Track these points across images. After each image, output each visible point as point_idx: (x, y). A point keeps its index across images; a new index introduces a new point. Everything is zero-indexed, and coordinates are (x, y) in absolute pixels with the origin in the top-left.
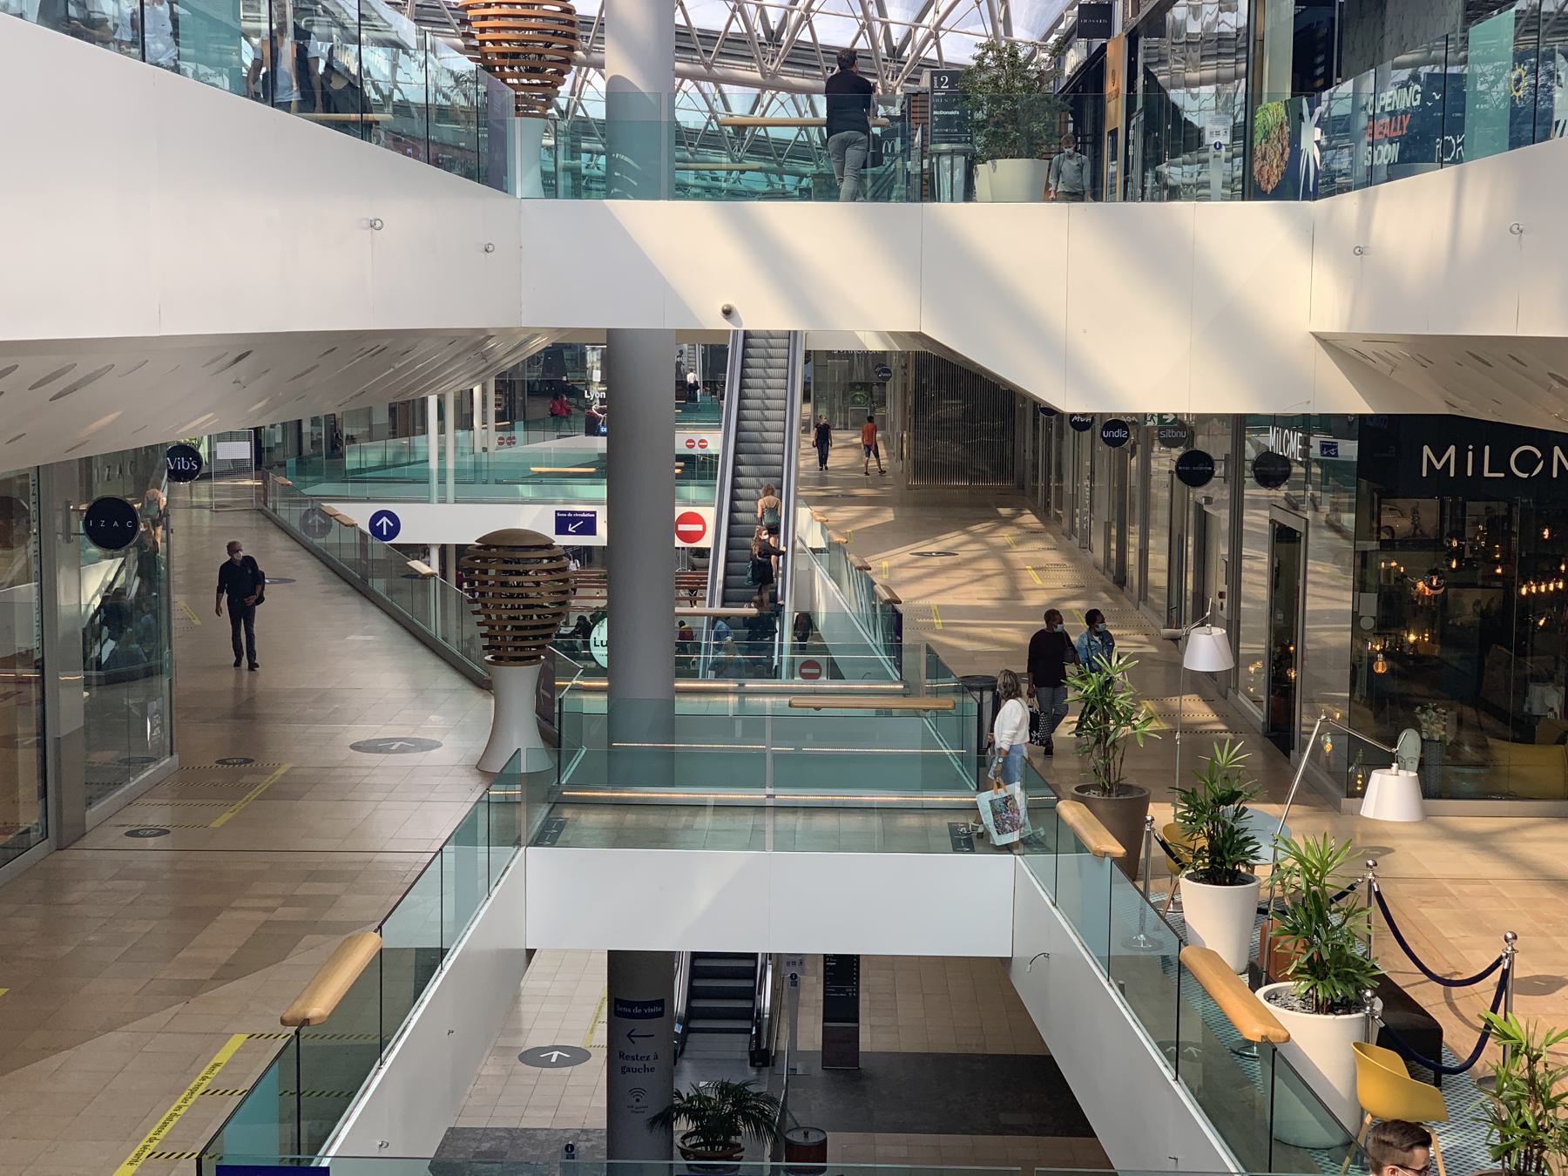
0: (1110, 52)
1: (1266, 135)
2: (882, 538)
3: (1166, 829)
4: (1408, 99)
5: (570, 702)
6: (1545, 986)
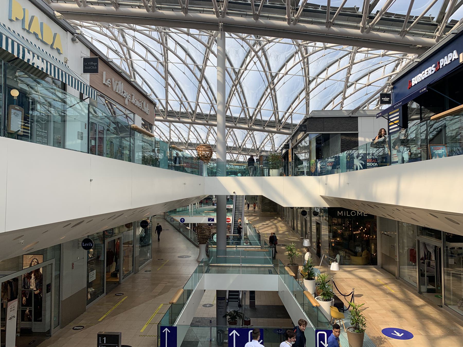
0: (289, 151)
1: (312, 165)
2: (257, 222)
3: (301, 271)
4: (333, 160)
5: (210, 249)
6: (360, 296)
